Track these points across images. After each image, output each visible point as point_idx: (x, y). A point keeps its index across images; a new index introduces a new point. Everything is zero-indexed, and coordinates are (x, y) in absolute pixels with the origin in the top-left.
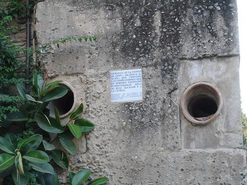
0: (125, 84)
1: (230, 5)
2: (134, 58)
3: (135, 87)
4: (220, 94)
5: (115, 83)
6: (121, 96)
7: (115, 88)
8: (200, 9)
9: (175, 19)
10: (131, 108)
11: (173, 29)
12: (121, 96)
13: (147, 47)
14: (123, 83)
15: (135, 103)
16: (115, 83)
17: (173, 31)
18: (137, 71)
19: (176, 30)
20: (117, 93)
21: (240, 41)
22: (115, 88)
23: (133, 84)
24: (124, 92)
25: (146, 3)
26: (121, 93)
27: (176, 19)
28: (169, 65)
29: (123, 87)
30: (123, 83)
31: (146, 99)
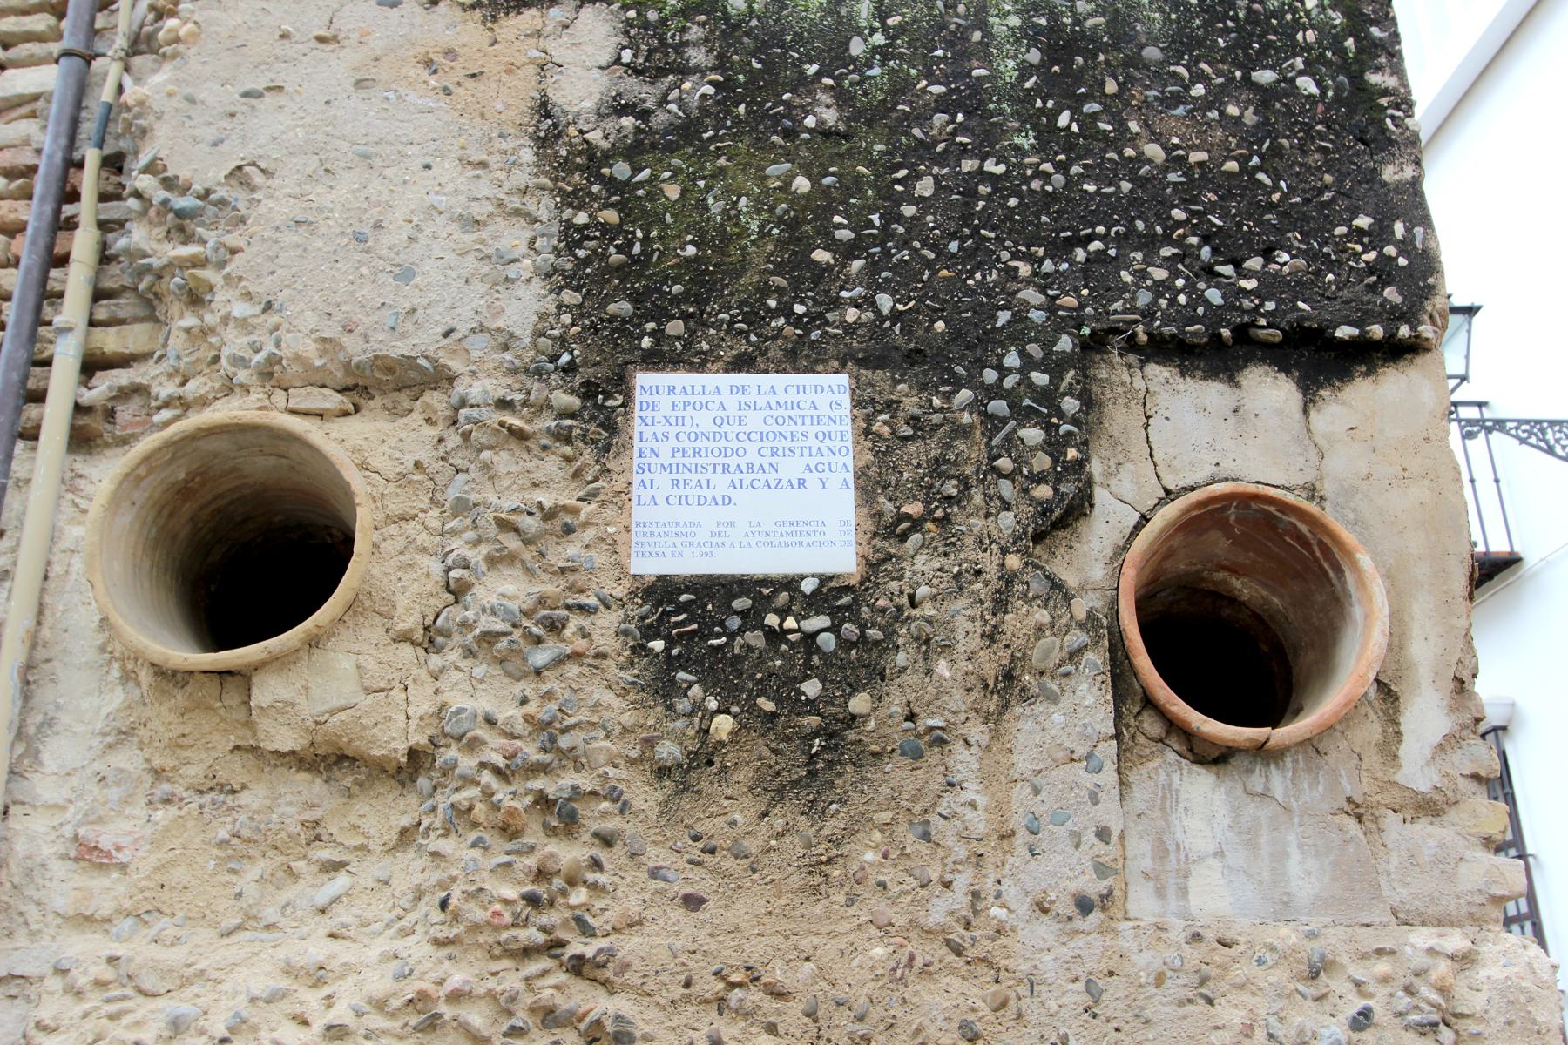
0: (733, 461)
1: (1431, 280)
2: (799, 309)
3: (802, 483)
4: (1364, 560)
5: (665, 449)
6: (702, 535)
7: (663, 480)
8: (1142, 275)
9: (1054, 115)
10: (772, 620)
11: (1047, 167)
12: (702, 535)
13: (887, 254)
14: (723, 452)
15: (808, 586)
16: (665, 449)
17: (1046, 177)
18: (818, 389)
19: (1066, 173)
20: (685, 513)
21: (1443, 258)
22: (663, 480)
23: (791, 468)
24: (722, 513)
25: (882, 14)
26: (709, 516)
27: (1064, 119)
28: (1028, 364)
29: (721, 482)
30: (723, 452)
31: (875, 566)
